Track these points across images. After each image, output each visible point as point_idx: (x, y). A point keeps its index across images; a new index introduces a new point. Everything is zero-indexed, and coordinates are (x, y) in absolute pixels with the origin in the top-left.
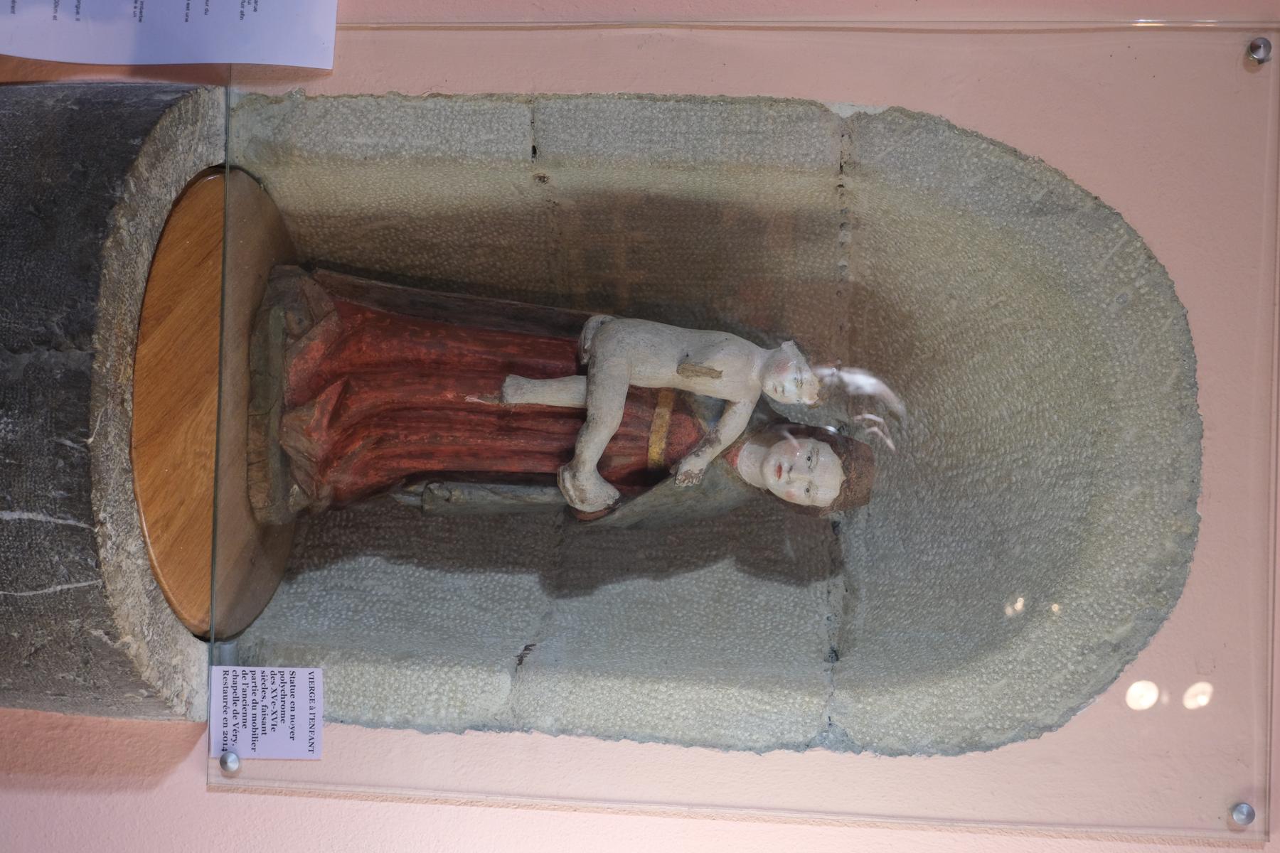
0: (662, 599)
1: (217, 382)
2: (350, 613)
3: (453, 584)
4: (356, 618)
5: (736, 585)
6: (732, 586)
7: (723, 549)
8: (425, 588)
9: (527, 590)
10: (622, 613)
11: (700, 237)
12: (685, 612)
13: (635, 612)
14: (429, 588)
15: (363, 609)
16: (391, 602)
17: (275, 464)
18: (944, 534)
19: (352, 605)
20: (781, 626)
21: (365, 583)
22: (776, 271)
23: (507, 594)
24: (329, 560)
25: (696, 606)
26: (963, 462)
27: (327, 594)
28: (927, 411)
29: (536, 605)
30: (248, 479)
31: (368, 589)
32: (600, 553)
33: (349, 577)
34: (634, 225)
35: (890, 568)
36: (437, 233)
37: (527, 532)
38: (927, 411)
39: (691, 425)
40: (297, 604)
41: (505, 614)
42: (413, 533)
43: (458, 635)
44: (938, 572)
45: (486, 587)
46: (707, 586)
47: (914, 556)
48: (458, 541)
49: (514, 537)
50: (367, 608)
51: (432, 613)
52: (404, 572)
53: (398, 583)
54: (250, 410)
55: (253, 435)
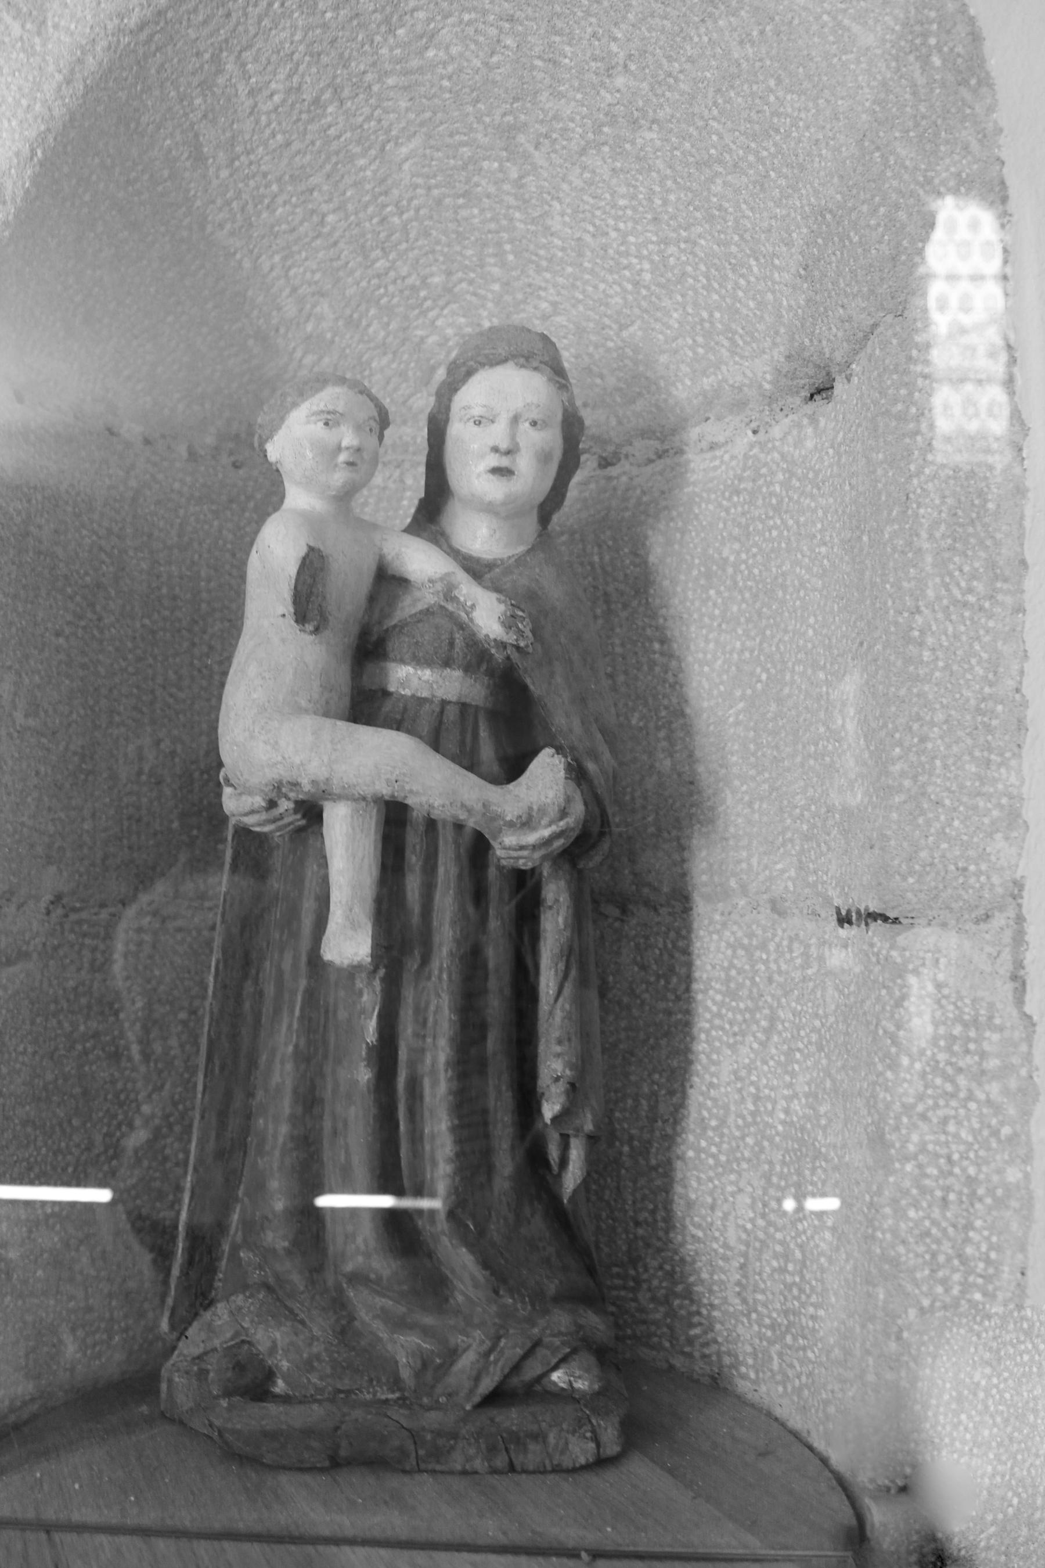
1: (334, 1549)
2: (790, 1267)
3: (728, 1084)
4: (798, 1254)
7: (649, 632)
8: (737, 1134)
9: (734, 952)
10: (767, 775)
13: (764, 755)
14: (738, 1127)
16: (765, 1192)
17: (511, 1418)
18: (605, 248)
19: (775, 1264)
20: (774, 501)
21: (732, 1242)
22: (196, 557)
23: (740, 986)
24: (694, 1308)
26: (489, 232)
27: (756, 1311)
28: (417, 311)
29: (759, 932)
32: (666, 835)
34: (105, 775)
35: (666, 342)
36: (120, 1117)
37: (635, 962)
38: (417, 311)
39: (420, 625)
40: (775, 1365)
42: (642, 1162)
43: (824, 1062)
44: (666, 241)
45: (731, 1024)
46: (711, 646)
47: (644, 298)
48: (653, 1082)
50: (779, 1236)
51: (782, 1116)
52: (711, 1174)
53: (731, 1183)
54: (408, 1468)
55: (457, 1462)
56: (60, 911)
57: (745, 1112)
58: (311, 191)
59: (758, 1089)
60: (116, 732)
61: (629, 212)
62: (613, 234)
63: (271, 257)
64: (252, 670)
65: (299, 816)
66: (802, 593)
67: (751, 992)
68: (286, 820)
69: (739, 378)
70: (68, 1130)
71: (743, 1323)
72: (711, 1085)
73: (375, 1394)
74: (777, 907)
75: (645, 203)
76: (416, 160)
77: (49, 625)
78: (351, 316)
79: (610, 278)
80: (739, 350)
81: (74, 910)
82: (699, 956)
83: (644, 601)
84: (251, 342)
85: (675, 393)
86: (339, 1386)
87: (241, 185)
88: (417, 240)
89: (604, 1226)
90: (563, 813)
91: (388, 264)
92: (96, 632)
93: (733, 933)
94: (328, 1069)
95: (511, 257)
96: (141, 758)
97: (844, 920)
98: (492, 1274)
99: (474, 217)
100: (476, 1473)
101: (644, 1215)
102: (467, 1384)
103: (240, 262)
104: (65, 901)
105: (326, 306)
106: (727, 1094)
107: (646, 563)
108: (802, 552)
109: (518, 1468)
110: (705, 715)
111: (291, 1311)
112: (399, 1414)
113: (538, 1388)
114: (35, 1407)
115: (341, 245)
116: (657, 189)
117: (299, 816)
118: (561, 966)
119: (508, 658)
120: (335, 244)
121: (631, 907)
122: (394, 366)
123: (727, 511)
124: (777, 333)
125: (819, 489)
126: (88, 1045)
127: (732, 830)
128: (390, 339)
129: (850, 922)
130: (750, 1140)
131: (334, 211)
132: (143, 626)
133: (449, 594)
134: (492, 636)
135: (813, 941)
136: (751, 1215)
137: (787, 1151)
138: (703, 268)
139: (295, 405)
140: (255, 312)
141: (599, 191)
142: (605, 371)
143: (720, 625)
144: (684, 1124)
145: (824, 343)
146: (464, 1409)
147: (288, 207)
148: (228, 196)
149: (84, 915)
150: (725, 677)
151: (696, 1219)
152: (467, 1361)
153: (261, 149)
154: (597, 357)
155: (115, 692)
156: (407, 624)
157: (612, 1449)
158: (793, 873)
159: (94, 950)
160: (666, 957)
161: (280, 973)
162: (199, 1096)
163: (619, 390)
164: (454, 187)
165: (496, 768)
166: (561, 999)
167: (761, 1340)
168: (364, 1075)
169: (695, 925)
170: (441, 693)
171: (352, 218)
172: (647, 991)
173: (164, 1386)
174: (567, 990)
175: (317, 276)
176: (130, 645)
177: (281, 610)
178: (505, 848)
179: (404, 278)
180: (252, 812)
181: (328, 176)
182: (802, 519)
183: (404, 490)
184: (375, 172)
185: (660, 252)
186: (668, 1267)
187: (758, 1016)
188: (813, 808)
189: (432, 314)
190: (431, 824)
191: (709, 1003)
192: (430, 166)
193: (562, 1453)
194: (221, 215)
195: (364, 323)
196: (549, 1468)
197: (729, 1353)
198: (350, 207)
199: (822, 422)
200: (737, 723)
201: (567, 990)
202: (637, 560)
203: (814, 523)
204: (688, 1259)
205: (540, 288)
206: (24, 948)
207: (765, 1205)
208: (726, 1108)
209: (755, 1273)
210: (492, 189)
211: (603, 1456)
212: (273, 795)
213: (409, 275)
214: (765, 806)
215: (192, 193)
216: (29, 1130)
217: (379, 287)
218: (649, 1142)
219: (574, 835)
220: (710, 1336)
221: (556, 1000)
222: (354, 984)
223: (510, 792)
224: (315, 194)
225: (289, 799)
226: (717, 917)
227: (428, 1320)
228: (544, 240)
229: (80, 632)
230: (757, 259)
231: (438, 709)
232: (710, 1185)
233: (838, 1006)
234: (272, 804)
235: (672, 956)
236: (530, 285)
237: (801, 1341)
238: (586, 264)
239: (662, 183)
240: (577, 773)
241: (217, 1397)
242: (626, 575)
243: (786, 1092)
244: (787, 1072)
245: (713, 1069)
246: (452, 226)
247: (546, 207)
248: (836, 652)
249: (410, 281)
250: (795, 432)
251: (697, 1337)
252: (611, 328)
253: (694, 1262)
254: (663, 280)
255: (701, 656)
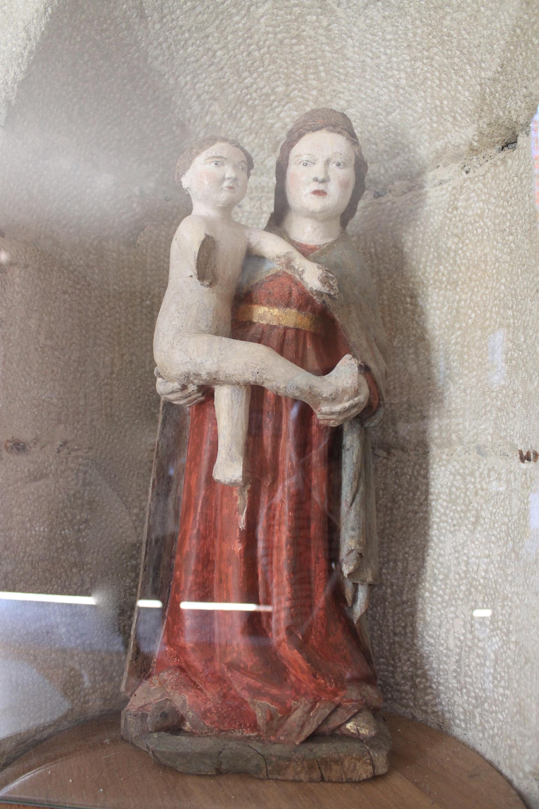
0: (457, 338)
3: (450, 554)
5: (439, 271)
6: (440, 274)
7: (404, 292)
8: (456, 584)
9: (454, 477)
10: (475, 373)
11: (107, 314)
12: (470, 312)
13: (473, 362)
14: (456, 579)
15: (483, 649)
18: (378, 66)
19: (478, 660)
21: (452, 646)
22: (144, 251)
23: (458, 497)
24: (428, 684)
25: (463, 303)
26: (311, 59)
27: (466, 687)
28: (269, 109)
29: (470, 465)
30: (339, 782)
31: (459, 644)
33: (445, 663)
35: (414, 121)
37: (395, 483)
40: (478, 720)
41: (482, 497)
42: (399, 599)
47: (401, 95)
49: (400, 497)
50: (480, 644)
52: (439, 606)
53: (451, 612)
54: (261, 777)
56: (66, 451)
57: (460, 571)
58: (207, 37)
59: (468, 558)
60: (98, 349)
61: (393, 43)
62: (383, 57)
63: (186, 77)
64: (173, 308)
65: (200, 394)
66: (497, 265)
67: (464, 500)
68: (193, 397)
69: (458, 140)
70: (70, 575)
71: (458, 695)
72: (440, 555)
73: (243, 734)
74: (481, 451)
75: (402, 36)
76: (268, 16)
77: (59, 287)
78: (231, 112)
79: (381, 84)
80: (458, 123)
81: (73, 450)
82: (433, 479)
83: (401, 274)
84: (174, 128)
85: (419, 151)
86: (222, 728)
87: (167, 33)
88: (269, 65)
89: (376, 635)
90: (357, 393)
91: (252, 81)
92: (87, 292)
93: (453, 466)
94: (217, 543)
95: (323, 74)
96: (113, 364)
97: (525, 458)
98: (312, 666)
99: (302, 50)
100: (301, 781)
101: (398, 630)
102: (297, 730)
103: (168, 80)
104: (69, 445)
105: (217, 106)
106: (449, 560)
107: (402, 252)
108: (496, 240)
109: (326, 779)
110: (437, 339)
111: (195, 683)
112: (257, 746)
113: (338, 732)
114: (51, 730)
115: (225, 69)
116: (410, 27)
117: (200, 394)
118: (355, 484)
119: (324, 302)
120: (222, 69)
121: (393, 451)
122: (256, 141)
123: (450, 220)
124: (482, 110)
125: (508, 202)
126: (82, 527)
127: (453, 406)
128: (254, 125)
129: (529, 460)
130: (463, 588)
131: (221, 49)
132: (114, 290)
133: (289, 263)
134: (314, 289)
135: (504, 471)
136: (464, 631)
137: (486, 594)
138: (437, 74)
139: (198, 154)
140: (177, 110)
141: (375, 31)
142: (378, 141)
143: (446, 287)
144: (423, 577)
145: (513, 112)
146: (294, 744)
147: (194, 47)
148: (160, 40)
149: (80, 453)
150: (449, 317)
151: (430, 632)
152: (296, 716)
153: (179, 11)
154: (373, 132)
155: (98, 326)
156: (264, 283)
157: (382, 770)
158: (491, 431)
159: (85, 473)
160: (413, 480)
161: (189, 488)
162: (143, 557)
163: (386, 152)
164: (290, 33)
165: (317, 367)
166: (354, 504)
167: (468, 705)
168: (238, 547)
169: (431, 461)
170: (284, 323)
171: (232, 53)
172: (402, 499)
173: (123, 722)
174: (358, 499)
175: (212, 88)
176: (106, 300)
177: (190, 273)
178: (322, 414)
179: (261, 89)
180: (173, 392)
181: (217, 28)
182: (497, 221)
183: (262, 213)
184: (244, 24)
185: (411, 66)
186: (413, 660)
187: (469, 515)
188: (504, 392)
189: (277, 110)
190: (278, 398)
191: (439, 507)
192: (276, 20)
193: (353, 771)
194: (157, 52)
195: (239, 116)
196: (344, 780)
197: (449, 712)
198: (230, 46)
199: (510, 162)
200: (456, 343)
201: (358, 499)
202: (397, 251)
203: (504, 223)
204: (425, 655)
205: (340, 92)
206: (44, 471)
207: (472, 626)
208: (449, 568)
209: (466, 666)
210: (312, 33)
211: (376, 773)
212: (184, 382)
213: (265, 87)
214: (473, 391)
215: (139, 38)
216: (47, 574)
217: (247, 94)
218: (403, 586)
219: (363, 406)
220: (437, 701)
221: (351, 505)
222: (232, 494)
223: (325, 380)
224: (210, 38)
225: (194, 384)
226: (444, 457)
227: (274, 691)
228: (343, 63)
229: (77, 292)
230: (470, 65)
231: (282, 332)
232: (439, 613)
233: (519, 510)
234: (184, 387)
235: (416, 479)
236: (334, 91)
237: (494, 708)
238: (367, 77)
239: (413, 23)
240: (365, 369)
241: (151, 732)
242: (390, 259)
243: (485, 560)
244: (486, 548)
245: (441, 545)
246: (289, 57)
247: (344, 43)
248: (519, 298)
249: (264, 91)
250: (492, 170)
251: (431, 701)
252: (381, 115)
253: (429, 657)
254: (413, 84)
255: (434, 305)
